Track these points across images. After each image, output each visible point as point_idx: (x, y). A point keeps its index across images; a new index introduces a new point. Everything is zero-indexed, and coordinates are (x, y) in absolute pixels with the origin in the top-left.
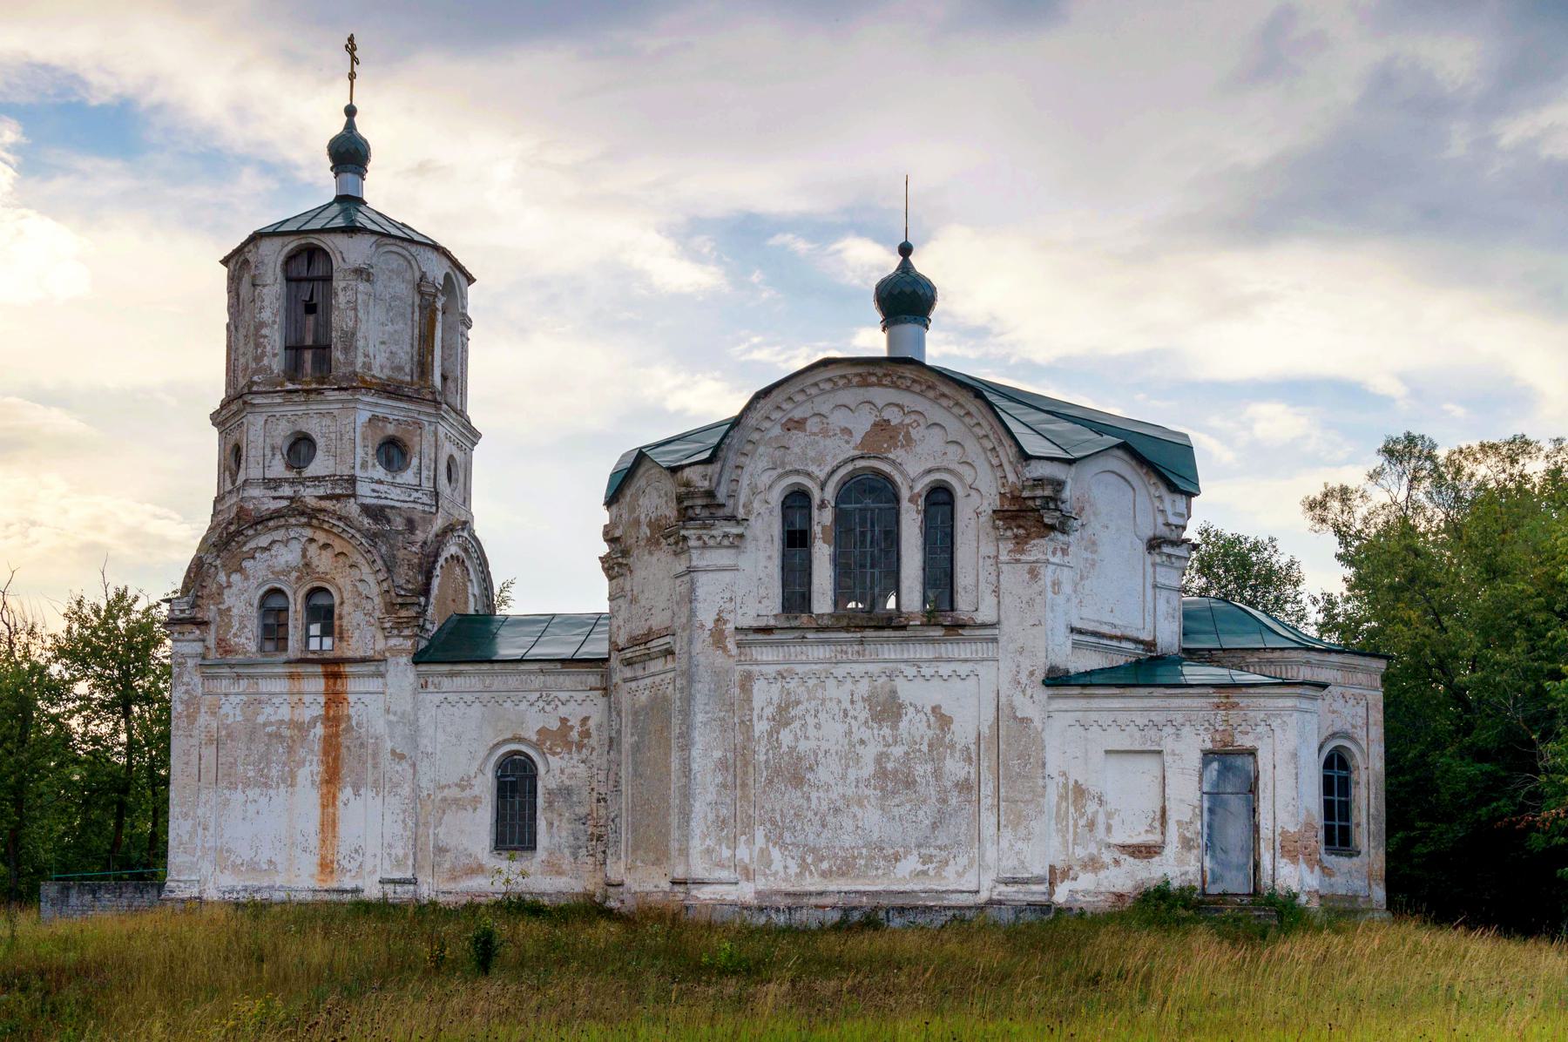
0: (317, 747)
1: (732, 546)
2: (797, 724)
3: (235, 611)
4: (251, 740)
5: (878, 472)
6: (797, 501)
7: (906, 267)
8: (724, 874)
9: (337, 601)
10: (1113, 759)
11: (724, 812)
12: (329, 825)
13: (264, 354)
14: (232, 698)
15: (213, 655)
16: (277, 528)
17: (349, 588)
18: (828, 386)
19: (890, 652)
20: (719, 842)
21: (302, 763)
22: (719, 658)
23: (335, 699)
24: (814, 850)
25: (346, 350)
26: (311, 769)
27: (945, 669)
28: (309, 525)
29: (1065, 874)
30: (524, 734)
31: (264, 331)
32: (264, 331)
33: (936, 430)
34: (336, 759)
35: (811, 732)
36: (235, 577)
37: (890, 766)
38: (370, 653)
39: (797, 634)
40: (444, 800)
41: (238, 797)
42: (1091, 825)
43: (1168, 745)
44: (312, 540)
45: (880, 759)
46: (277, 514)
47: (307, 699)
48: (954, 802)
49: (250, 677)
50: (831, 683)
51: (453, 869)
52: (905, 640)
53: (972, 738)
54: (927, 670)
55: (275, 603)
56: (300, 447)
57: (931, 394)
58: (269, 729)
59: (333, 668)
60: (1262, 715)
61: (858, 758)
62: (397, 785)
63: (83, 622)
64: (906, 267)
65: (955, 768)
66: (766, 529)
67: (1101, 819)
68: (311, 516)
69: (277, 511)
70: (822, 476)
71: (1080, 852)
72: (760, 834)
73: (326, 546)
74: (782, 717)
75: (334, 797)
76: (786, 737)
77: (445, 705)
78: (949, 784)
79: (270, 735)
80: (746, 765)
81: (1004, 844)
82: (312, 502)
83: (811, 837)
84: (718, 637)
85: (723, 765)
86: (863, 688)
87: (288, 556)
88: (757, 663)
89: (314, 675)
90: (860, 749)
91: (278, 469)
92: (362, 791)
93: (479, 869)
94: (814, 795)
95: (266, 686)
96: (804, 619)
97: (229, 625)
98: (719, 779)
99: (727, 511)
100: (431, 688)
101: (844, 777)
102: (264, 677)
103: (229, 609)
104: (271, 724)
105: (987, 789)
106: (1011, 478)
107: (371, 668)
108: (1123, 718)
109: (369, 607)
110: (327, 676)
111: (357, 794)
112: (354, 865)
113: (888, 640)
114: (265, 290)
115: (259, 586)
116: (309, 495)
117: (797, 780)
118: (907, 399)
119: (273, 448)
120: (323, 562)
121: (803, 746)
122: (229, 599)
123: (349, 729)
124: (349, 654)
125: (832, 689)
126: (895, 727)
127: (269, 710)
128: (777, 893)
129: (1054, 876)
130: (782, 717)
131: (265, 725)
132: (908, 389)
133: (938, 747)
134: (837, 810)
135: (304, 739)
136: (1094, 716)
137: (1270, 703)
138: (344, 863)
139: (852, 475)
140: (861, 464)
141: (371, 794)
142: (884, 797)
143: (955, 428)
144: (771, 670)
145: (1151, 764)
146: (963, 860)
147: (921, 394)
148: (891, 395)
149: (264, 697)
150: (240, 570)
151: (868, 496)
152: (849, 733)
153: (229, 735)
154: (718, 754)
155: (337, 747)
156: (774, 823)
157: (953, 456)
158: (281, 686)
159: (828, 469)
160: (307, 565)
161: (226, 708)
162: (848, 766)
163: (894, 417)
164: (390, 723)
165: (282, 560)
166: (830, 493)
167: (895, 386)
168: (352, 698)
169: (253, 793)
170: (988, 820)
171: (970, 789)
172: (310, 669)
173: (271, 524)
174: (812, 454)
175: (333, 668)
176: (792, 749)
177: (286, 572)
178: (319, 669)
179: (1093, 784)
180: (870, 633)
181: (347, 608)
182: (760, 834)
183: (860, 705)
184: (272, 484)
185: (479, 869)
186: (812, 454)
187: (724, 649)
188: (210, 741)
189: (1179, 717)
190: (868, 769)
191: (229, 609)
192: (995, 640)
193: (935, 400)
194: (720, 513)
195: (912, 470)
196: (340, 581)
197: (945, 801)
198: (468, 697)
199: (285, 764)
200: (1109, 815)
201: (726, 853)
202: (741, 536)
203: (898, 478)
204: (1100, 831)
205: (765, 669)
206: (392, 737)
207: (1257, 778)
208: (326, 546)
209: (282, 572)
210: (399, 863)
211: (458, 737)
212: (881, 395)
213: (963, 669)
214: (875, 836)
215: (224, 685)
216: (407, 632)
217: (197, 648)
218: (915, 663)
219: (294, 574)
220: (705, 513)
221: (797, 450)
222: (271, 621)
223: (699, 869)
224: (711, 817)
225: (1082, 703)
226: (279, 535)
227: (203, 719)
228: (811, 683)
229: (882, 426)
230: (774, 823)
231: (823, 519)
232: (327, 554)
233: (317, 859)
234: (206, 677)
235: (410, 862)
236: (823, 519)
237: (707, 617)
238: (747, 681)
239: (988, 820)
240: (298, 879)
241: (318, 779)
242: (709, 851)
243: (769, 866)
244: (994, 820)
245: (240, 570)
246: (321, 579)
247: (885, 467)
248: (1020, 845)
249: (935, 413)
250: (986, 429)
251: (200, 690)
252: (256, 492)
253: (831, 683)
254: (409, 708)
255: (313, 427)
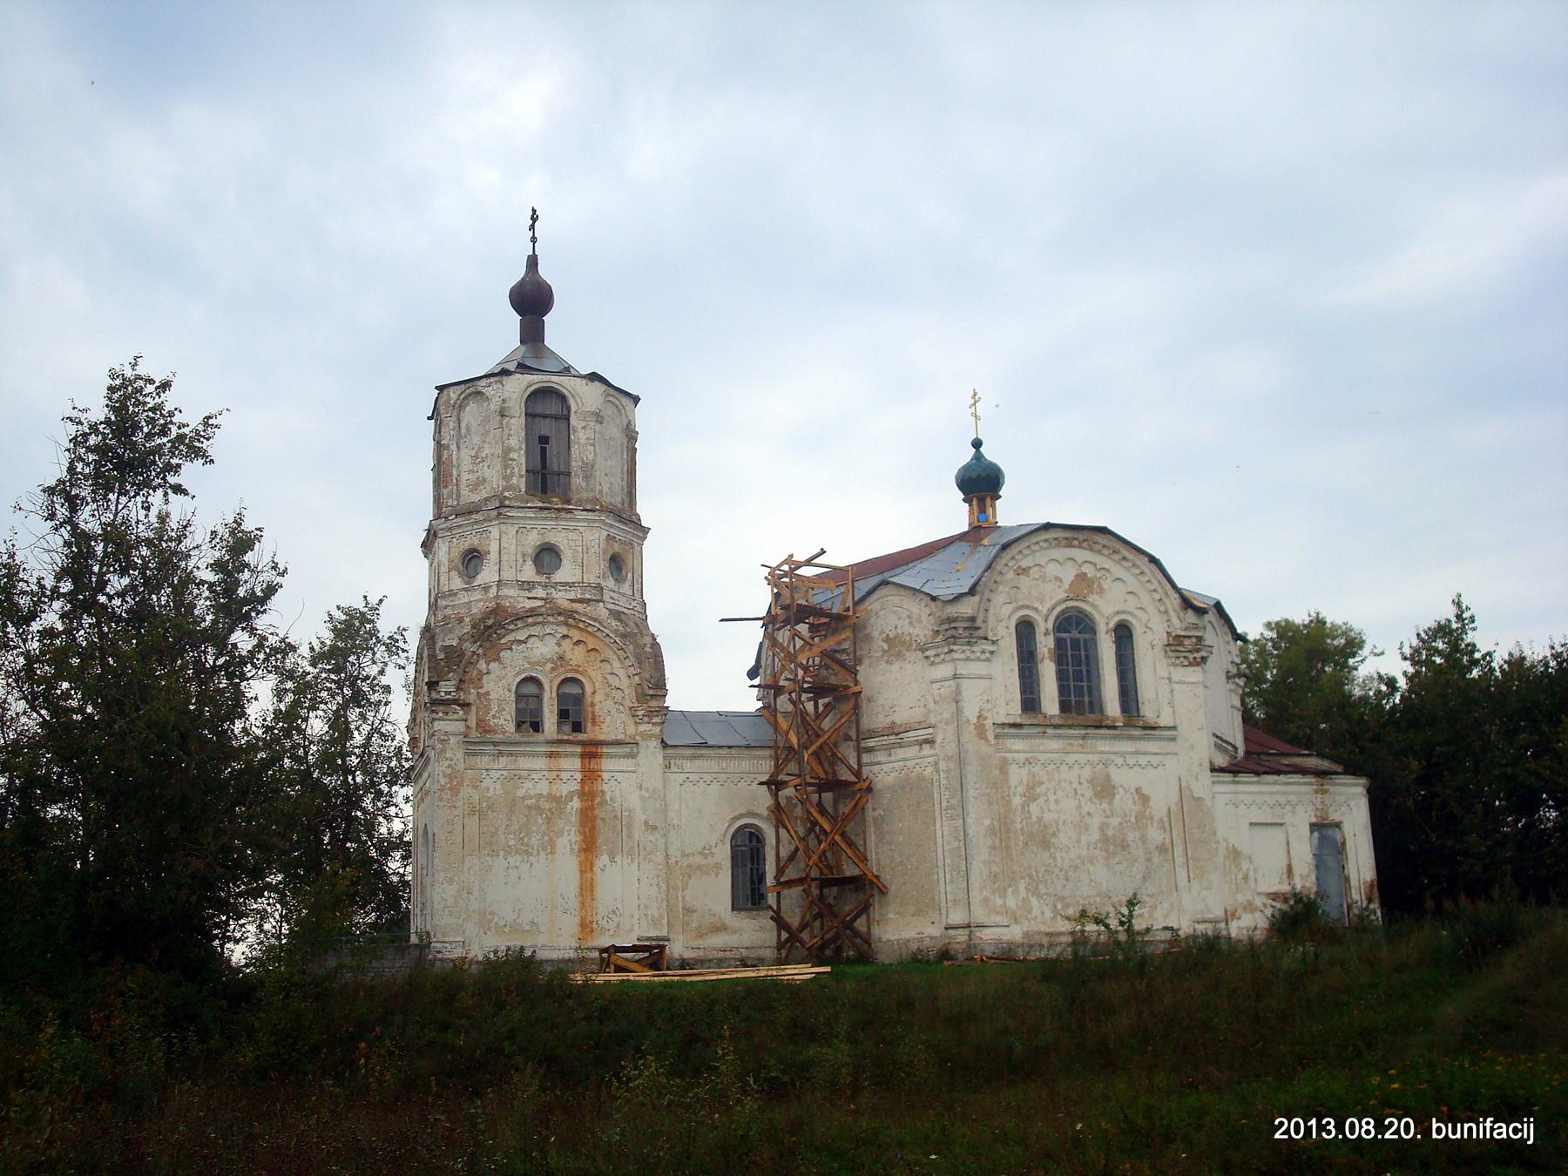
0: (574, 818)
1: (988, 660)
2: (1041, 800)
3: (493, 696)
4: (512, 811)
5: (1080, 611)
6: (1025, 630)
7: (978, 457)
8: (998, 919)
9: (588, 689)
10: (1256, 829)
11: (995, 868)
12: (587, 889)
13: (512, 474)
14: (492, 773)
15: (474, 734)
16: (535, 624)
17: (600, 679)
18: (1045, 545)
19: (1103, 746)
20: (993, 892)
21: (560, 834)
22: (983, 748)
23: (590, 776)
24: (1062, 899)
25: (587, 478)
26: (569, 839)
27: (1143, 760)
28: (566, 624)
29: (1233, 915)
30: (755, 810)
31: (512, 455)
32: (512, 455)
33: (1118, 583)
34: (593, 827)
35: (1053, 806)
36: (494, 665)
37: (1110, 833)
38: (621, 737)
39: (1039, 730)
40: (690, 866)
41: (500, 863)
42: (1246, 878)
43: (1289, 819)
44: (565, 637)
45: (1103, 827)
46: (532, 612)
47: (565, 775)
48: (1156, 860)
49: (510, 754)
50: (1064, 768)
51: (699, 928)
52: (1116, 737)
53: (1164, 813)
54: (1131, 761)
55: (530, 689)
56: (547, 556)
57: (1116, 557)
58: (528, 802)
59: (591, 751)
60: (1343, 799)
61: (1087, 827)
62: (652, 853)
63: (1239, 675)
64: (978, 457)
65: (1155, 835)
66: (1009, 645)
67: (1251, 873)
68: (568, 617)
69: (532, 610)
70: (1044, 610)
71: (1241, 898)
72: (1022, 886)
73: (579, 642)
74: (1030, 795)
75: (592, 864)
76: (1034, 809)
77: (687, 784)
78: (1152, 847)
79: (529, 807)
80: (1008, 831)
81: (1194, 892)
82: (566, 605)
83: (1059, 888)
84: (981, 731)
85: (991, 831)
86: (1087, 772)
87: (543, 649)
88: (1011, 751)
89: (572, 755)
90: (1088, 819)
91: (529, 572)
92: (618, 859)
93: (720, 928)
94: (1058, 855)
95: (525, 763)
96: (1039, 719)
97: (488, 708)
98: (990, 842)
99: (980, 633)
100: (674, 769)
101: (1078, 841)
102: (524, 755)
103: (488, 693)
104: (530, 797)
105: (1179, 850)
106: (1175, 621)
107: (627, 750)
108: (1259, 799)
109: (619, 695)
110: (583, 756)
111: (612, 861)
112: (612, 925)
113: (1103, 737)
114: (513, 421)
115: (518, 674)
116: (562, 598)
117: (1045, 844)
118: (1102, 561)
119: (524, 555)
120: (576, 656)
121: (1047, 817)
122: (488, 684)
123: (604, 803)
124: (602, 737)
125: (1064, 773)
126: (1110, 803)
127: (528, 784)
128: (1039, 933)
129: (1229, 916)
130: (1030, 795)
131: (524, 798)
132: (1099, 552)
133: (1142, 819)
134: (1076, 868)
135: (562, 811)
136: (1241, 797)
137: (1343, 789)
138: (603, 923)
139: (1063, 612)
140: (1072, 604)
141: (627, 861)
142: (1108, 858)
143: (1132, 582)
144: (1021, 757)
145: (1278, 834)
146: (1166, 905)
147: (1109, 556)
148: (1088, 555)
149: (525, 773)
150: (498, 659)
151: (1074, 629)
152: (1079, 807)
153: (489, 807)
154: (987, 822)
155: (594, 818)
156: (1031, 877)
157: (1131, 604)
158: (541, 763)
159: (1048, 605)
160: (561, 658)
161: (487, 782)
162: (1080, 833)
163: (1089, 571)
164: (642, 798)
165: (537, 653)
166: (1050, 625)
167: (1091, 549)
168: (606, 776)
169: (514, 860)
170: (1181, 874)
171: (1166, 850)
172: (570, 749)
173: (530, 620)
174: (1035, 594)
175: (591, 751)
176: (1040, 819)
177: (540, 663)
178: (579, 749)
179: (1244, 847)
180: (1091, 731)
181: (599, 698)
182: (1022, 886)
183: (1085, 785)
184: (528, 586)
185: (720, 928)
186: (1035, 594)
187: (986, 740)
188: (473, 812)
189: (1294, 799)
190: (1095, 835)
191: (488, 693)
192: (1174, 739)
193: (1118, 562)
194: (978, 633)
195: (1105, 610)
196: (593, 674)
197: (1150, 860)
198: (707, 777)
199: (544, 834)
200: (1255, 871)
201: (999, 902)
202: (992, 652)
203: (1096, 616)
204: (1252, 882)
205: (1016, 756)
206: (644, 810)
207: (1344, 844)
208: (579, 642)
209: (538, 663)
210: (655, 923)
211: (700, 811)
212: (1079, 554)
213: (1155, 760)
214: (1104, 888)
215: (484, 761)
216: (655, 720)
217: (460, 726)
218: (1123, 754)
219: (549, 665)
220: (966, 634)
221: (1025, 590)
222: (523, 706)
223: (979, 915)
224: (986, 873)
225: (1232, 788)
226: (535, 630)
227: (466, 791)
228: (1050, 768)
229: (1082, 577)
230: (1031, 877)
231: (1045, 644)
232: (580, 649)
233: (577, 920)
234: (468, 754)
235: (665, 922)
236: (1045, 644)
237: (971, 713)
238: (1004, 766)
239: (1181, 874)
240: (555, 940)
241: (576, 847)
242: (986, 900)
243: (1030, 911)
244: (1185, 874)
245: (498, 659)
246: (576, 671)
247: (1088, 608)
248: (1205, 893)
249: (1117, 571)
250: (1155, 585)
251: (461, 766)
252: (510, 592)
253: (1064, 768)
254: (659, 785)
255: (559, 538)
